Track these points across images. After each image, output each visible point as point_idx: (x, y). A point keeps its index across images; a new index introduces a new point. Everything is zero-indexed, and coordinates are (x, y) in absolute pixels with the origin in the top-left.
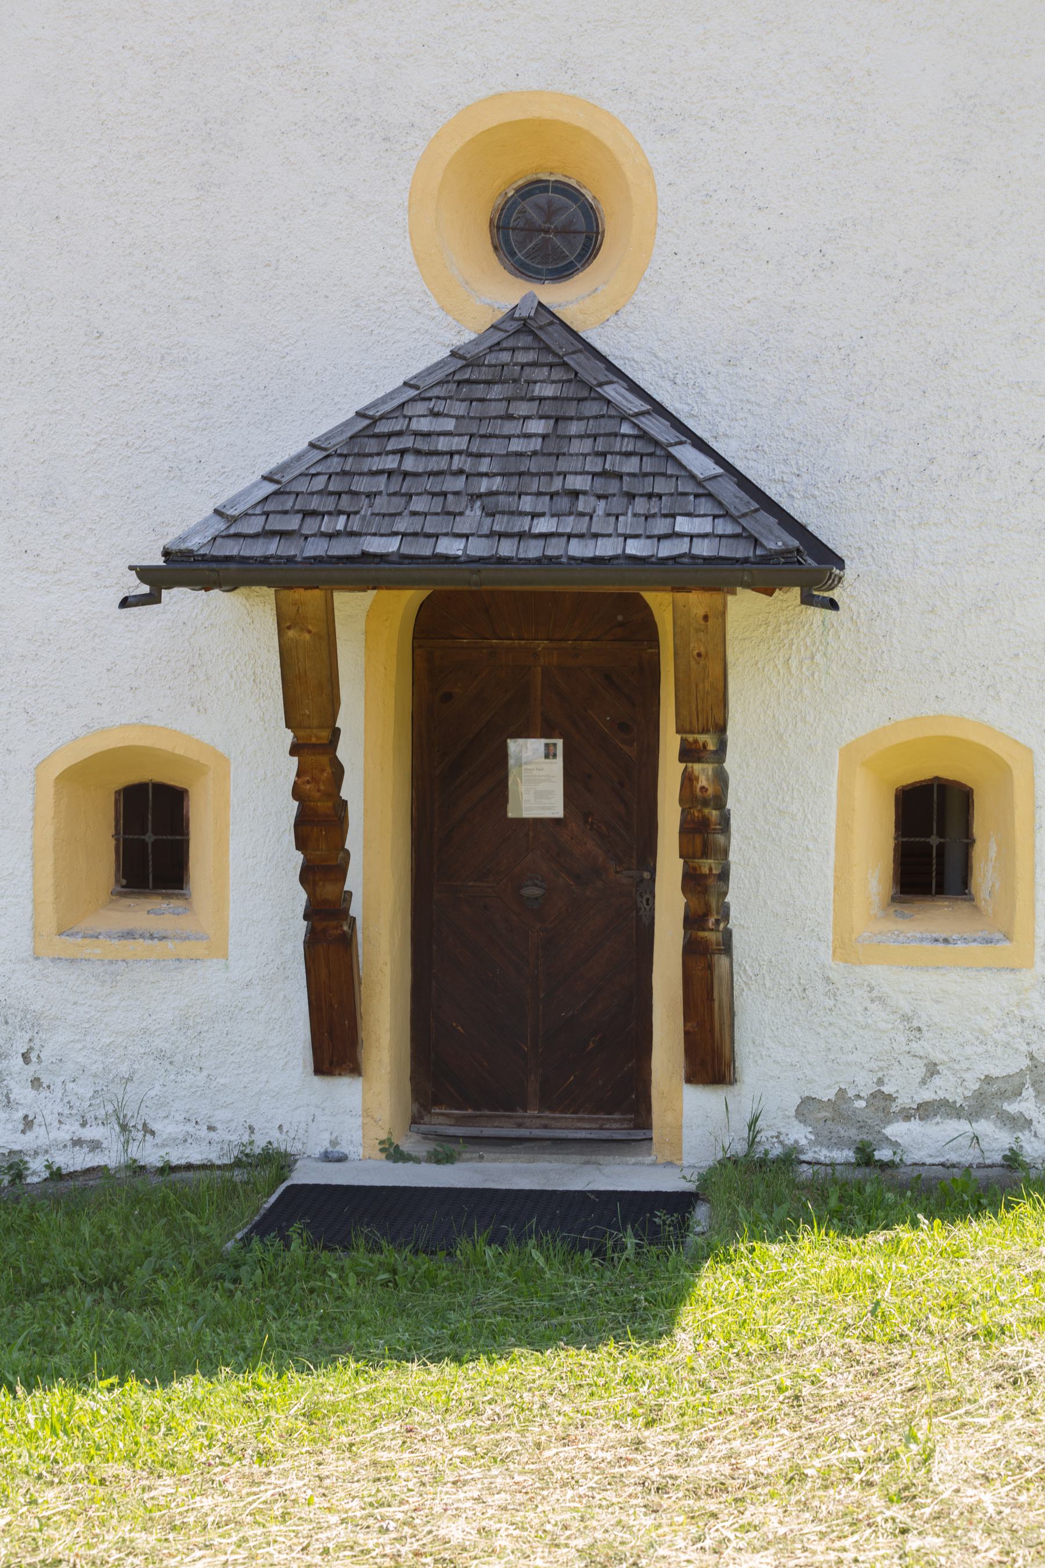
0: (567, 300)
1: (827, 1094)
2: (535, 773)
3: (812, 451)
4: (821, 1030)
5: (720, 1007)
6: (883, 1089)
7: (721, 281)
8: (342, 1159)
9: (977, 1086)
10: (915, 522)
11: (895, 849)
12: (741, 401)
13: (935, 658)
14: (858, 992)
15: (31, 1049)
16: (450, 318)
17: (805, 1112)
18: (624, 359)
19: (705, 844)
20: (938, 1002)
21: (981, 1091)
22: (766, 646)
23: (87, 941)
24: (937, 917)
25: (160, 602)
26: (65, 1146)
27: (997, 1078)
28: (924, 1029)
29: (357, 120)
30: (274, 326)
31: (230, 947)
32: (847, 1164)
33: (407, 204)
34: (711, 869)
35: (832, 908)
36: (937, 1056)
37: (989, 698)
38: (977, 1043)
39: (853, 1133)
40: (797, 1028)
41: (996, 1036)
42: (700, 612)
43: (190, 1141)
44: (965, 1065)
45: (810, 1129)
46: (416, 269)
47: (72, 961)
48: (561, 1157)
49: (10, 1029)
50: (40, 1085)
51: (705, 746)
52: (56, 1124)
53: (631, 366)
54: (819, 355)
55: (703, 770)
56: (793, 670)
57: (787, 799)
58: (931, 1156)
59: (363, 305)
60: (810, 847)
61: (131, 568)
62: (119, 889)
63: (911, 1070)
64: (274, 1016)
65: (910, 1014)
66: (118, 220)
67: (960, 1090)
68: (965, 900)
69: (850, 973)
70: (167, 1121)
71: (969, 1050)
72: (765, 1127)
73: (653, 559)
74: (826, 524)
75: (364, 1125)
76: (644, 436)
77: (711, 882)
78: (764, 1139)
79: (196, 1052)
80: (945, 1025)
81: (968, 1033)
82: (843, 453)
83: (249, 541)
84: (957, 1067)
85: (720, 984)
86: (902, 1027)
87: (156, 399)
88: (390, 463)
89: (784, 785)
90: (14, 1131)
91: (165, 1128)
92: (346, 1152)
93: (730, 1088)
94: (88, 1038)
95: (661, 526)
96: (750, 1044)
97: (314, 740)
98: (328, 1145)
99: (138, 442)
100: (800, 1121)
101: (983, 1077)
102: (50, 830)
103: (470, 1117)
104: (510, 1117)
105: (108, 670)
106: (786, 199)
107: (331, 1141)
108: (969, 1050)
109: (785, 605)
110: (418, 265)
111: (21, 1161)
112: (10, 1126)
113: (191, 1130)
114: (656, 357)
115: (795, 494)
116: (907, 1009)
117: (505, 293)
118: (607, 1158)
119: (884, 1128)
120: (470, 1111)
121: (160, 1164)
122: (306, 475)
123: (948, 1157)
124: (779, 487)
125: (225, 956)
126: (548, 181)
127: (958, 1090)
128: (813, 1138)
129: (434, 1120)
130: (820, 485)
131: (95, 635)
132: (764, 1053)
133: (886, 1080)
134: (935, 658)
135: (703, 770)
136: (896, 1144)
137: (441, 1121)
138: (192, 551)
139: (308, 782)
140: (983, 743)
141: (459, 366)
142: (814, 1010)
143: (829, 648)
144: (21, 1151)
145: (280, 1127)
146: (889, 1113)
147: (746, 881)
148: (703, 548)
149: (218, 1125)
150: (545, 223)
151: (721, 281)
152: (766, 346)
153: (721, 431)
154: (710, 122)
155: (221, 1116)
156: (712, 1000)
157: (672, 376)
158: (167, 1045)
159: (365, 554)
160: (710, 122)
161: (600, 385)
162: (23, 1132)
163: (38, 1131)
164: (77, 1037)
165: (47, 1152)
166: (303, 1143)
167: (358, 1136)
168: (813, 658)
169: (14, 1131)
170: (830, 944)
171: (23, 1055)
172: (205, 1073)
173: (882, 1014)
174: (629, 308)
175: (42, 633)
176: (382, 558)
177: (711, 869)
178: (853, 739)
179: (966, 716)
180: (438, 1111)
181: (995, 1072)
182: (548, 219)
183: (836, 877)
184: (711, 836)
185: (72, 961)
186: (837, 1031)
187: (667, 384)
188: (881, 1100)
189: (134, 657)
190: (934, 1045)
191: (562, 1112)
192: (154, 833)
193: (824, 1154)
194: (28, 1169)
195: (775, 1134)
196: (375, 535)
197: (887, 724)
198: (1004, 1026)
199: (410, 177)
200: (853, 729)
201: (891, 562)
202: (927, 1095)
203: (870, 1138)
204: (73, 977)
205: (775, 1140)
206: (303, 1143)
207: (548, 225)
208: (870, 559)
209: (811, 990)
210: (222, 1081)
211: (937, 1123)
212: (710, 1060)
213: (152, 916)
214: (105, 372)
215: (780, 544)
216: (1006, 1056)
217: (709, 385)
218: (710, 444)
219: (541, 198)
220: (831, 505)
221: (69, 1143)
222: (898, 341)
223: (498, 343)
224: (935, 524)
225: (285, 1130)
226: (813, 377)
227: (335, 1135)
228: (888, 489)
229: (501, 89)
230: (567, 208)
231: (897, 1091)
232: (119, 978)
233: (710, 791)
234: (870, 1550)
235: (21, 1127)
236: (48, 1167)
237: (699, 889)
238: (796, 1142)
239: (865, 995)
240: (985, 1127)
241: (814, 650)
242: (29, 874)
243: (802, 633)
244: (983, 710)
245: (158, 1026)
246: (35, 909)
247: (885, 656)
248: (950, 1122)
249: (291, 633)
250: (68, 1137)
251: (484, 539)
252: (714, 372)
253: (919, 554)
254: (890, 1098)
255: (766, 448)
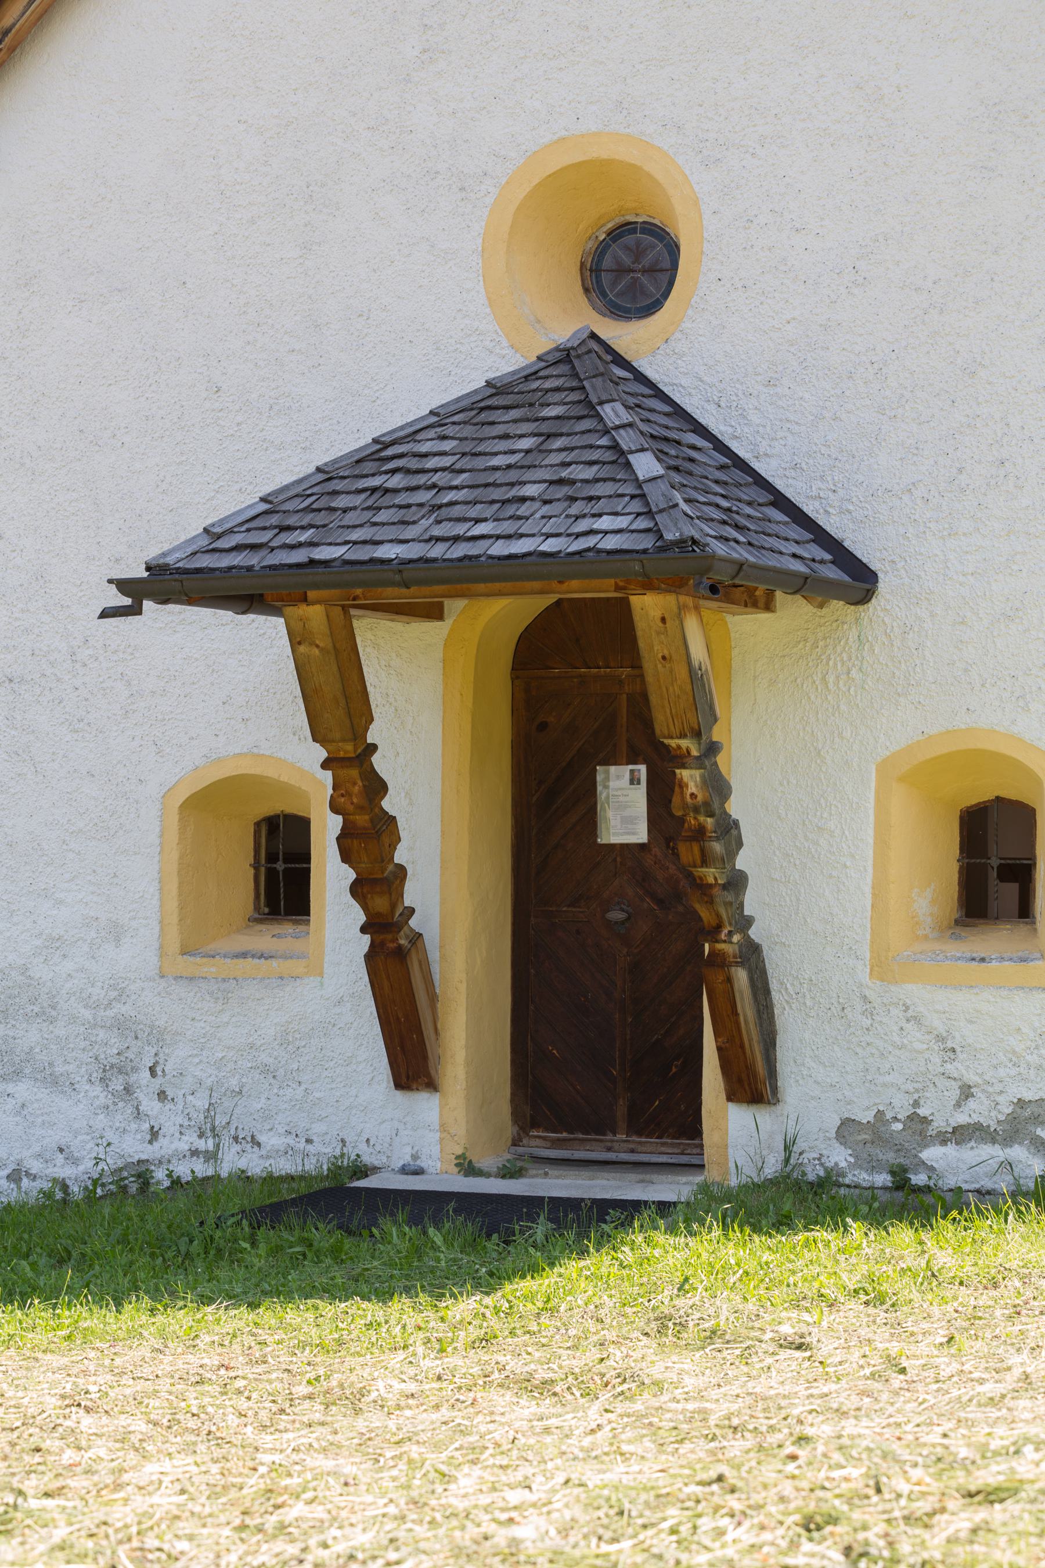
0: (625, 336)
1: (867, 1117)
2: (621, 799)
3: (848, 467)
4: (858, 1050)
5: (746, 1021)
6: (919, 1111)
7: (761, 303)
8: (419, 1172)
9: (1009, 1110)
10: (945, 533)
11: (960, 872)
12: (781, 420)
13: (966, 670)
14: (895, 1011)
15: (156, 1063)
16: (518, 355)
17: (846, 1134)
18: (673, 385)
19: (703, 852)
20: (971, 1022)
21: (1015, 1115)
22: (805, 663)
23: (205, 960)
24: (996, 940)
25: (140, 613)
26: (185, 1156)
27: (1030, 1101)
28: (958, 1049)
29: (437, 173)
30: (366, 372)
31: (326, 965)
32: (885, 1188)
33: (480, 249)
34: (716, 879)
35: (869, 926)
36: (971, 1078)
37: (1019, 709)
38: (1010, 1065)
39: (890, 1157)
40: (836, 1048)
41: (1029, 1058)
42: (657, 614)
43: (290, 1152)
44: (998, 1087)
45: (850, 1152)
46: (488, 310)
47: (191, 979)
48: (618, 1175)
49: (139, 1043)
50: (166, 1098)
51: (688, 752)
52: (177, 1135)
53: (679, 392)
54: (853, 370)
55: (691, 776)
56: (831, 685)
57: (825, 815)
58: (966, 1182)
59: (442, 347)
60: (848, 864)
61: (110, 581)
62: (257, 916)
63: (946, 1093)
64: (362, 1032)
65: (945, 1034)
66: (234, 282)
67: (993, 1114)
68: (1027, 923)
69: (886, 992)
70: (271, 1133)
71: (1002, 1072)
72: (807, 1149)
73: (562, 555)
74: (860, 538)
75: (441, 1140)
76: (615, 447)
77: (716, 891)
78: (806, 1161)
79: (295, 1066)
80: (978, 1046)
81: (1001, 1054)
82: (876, 467)
83: (224, 554)
84: (990, 1089)
85: (742, 999)
86: (937, 1048)
87: (264, 447)
88: (376, 482)
89: (822, 801)
90: (142, 1141)
91: (271, 1141)
92: (423, 1165)
93: (773, 1108)
94: (204, 1053)
95: (582, 526)
96: (792, 1063)
97: (342, 754)
98: (410, 1159)
99: (250, 488)
100: (841, 1143)
101: (1015, 1101)
102: (175, 855)
103: (564, 1140)
104: (601, 1141)
105: (224, 703)
106: (822, 219)
107: (412, 1156)
108: (1002, 1072)
109: (823, 621)
110: (491, 306)
111: (147, 1170)
112: (139, 1137)
113: (292, 1142)
114: (702, 381)
115: (831, 510)
116: (942, 1030)
117: (566, 318)
118: (660, 1177)
119: (921, 1151)
120: (565, 1135)
121: (264, 1175)
122: (302, 496)
123: (983, 1183)
124: (817, 504)
125: (321, 975)
126: (636, 223)
127: (992, 1114)
128: (852, 1160)
129: (533, 1143)
130: (854, 500)
131: (213, 670)
132: (805, 1073)
133: (922, 1102)
134: (966, 670)
135: (691, 776)
136: (932, 1169)
137: (537, 1145)
138: (168, 565)
139: (343, 795)
140: (1014, 755)
141: (488, 394)
142: (852, 1030)
143: (865, 663)
144: (148, 1161)
145: (368, 1140)
146: (926, 1137)
147: (788, 899)
148: (610, 543)
149: (315, 1138)
150: (633, 263)
151: (761, 303)
152: (804, 364)
153: (762, 451)
154: (751, 150)
155: (318, 1128)
156: (737, 1014)
157: (716, 399)
158: (271, 1060)
159: (312, 562)
160: (751, 150)
161: (601, 403)
162: (150, 1142)
163: (162, 1141)
164: (195, 1052)
165: (169, 1161)
166: (388, 1157)
167: (436, 1150)
168: (848, 673)
169: (142, 1141)
170: (868, 963)
171: (150, 1068)
172: (303, 1087)
173: (918, 1034)
174: (678, 335)
175: (168, 670)
176: (383, 561)
177: (716, 879)
178: (888, 753)
179: (997, 729)
180: (536, 1134)
181: (1028, 1096)
182: (637, 260)
183: (874, 894)
184: (707, 844)
185: (191, 979)
186: (874, 1051)
187: (712, 408)
188: (918, 1122)
189: (246, 690)
190: (968, 1067)
191: (647, 1137)
192: (285, 862)
193: (864, 1177)
194: (153, 1177)
195: (816, 1156)
196: (330, 544)
197: (921, 738)
198: (1037, 1048)
199: (483, 223)
200: (888, 744)
201: (922, 574)
202: (961, 1118)
203: (908, 1162)
204: (192, 994)
205: (817, 1162)
206: (388, 1157)
207: (632, 262)
208: (903, 571)
209: (849, 1009)
210: (317, 1095)
211: (972, 1148)
212: (752, 1085)
213: (275, 939)
214: (223, 423)
215: (677, 534)
216: (1039, 1079)
217: (751, 406)
218: (752, 465)
219: (629, 239)
220: (865, 520)
221: (188, 1154)
222: (928, 352)
223: (536, 372)
224: (964, 534)
225: (371, 1143)
226: (847, 393)
227: (416, 1149)
228: (919, 501)
229: (563, 133)
230: (654, 247)
231: (933, 1114)
232: (230, 995)
233: (700, 798)
234: (511, 1487)
235: (148, 1137)
236: (169, 1176)
237: (706, 899)
238: (836, 1164)
239: (901, 1015)
240: (1018, 1153)
241: (850, 665)
242: (157, 897)
243: (839, 649)
244: (1014, 722)
245: (263, 1041)
246: (162, 930)
247: (918, 669)
248: (985, 1147)
249: (302, 649)
250: (187, 1147)
251: (422, 544)
252: (755, 393)
253: (949, 565)
254: (925, 1121)
255: (804, 465)
